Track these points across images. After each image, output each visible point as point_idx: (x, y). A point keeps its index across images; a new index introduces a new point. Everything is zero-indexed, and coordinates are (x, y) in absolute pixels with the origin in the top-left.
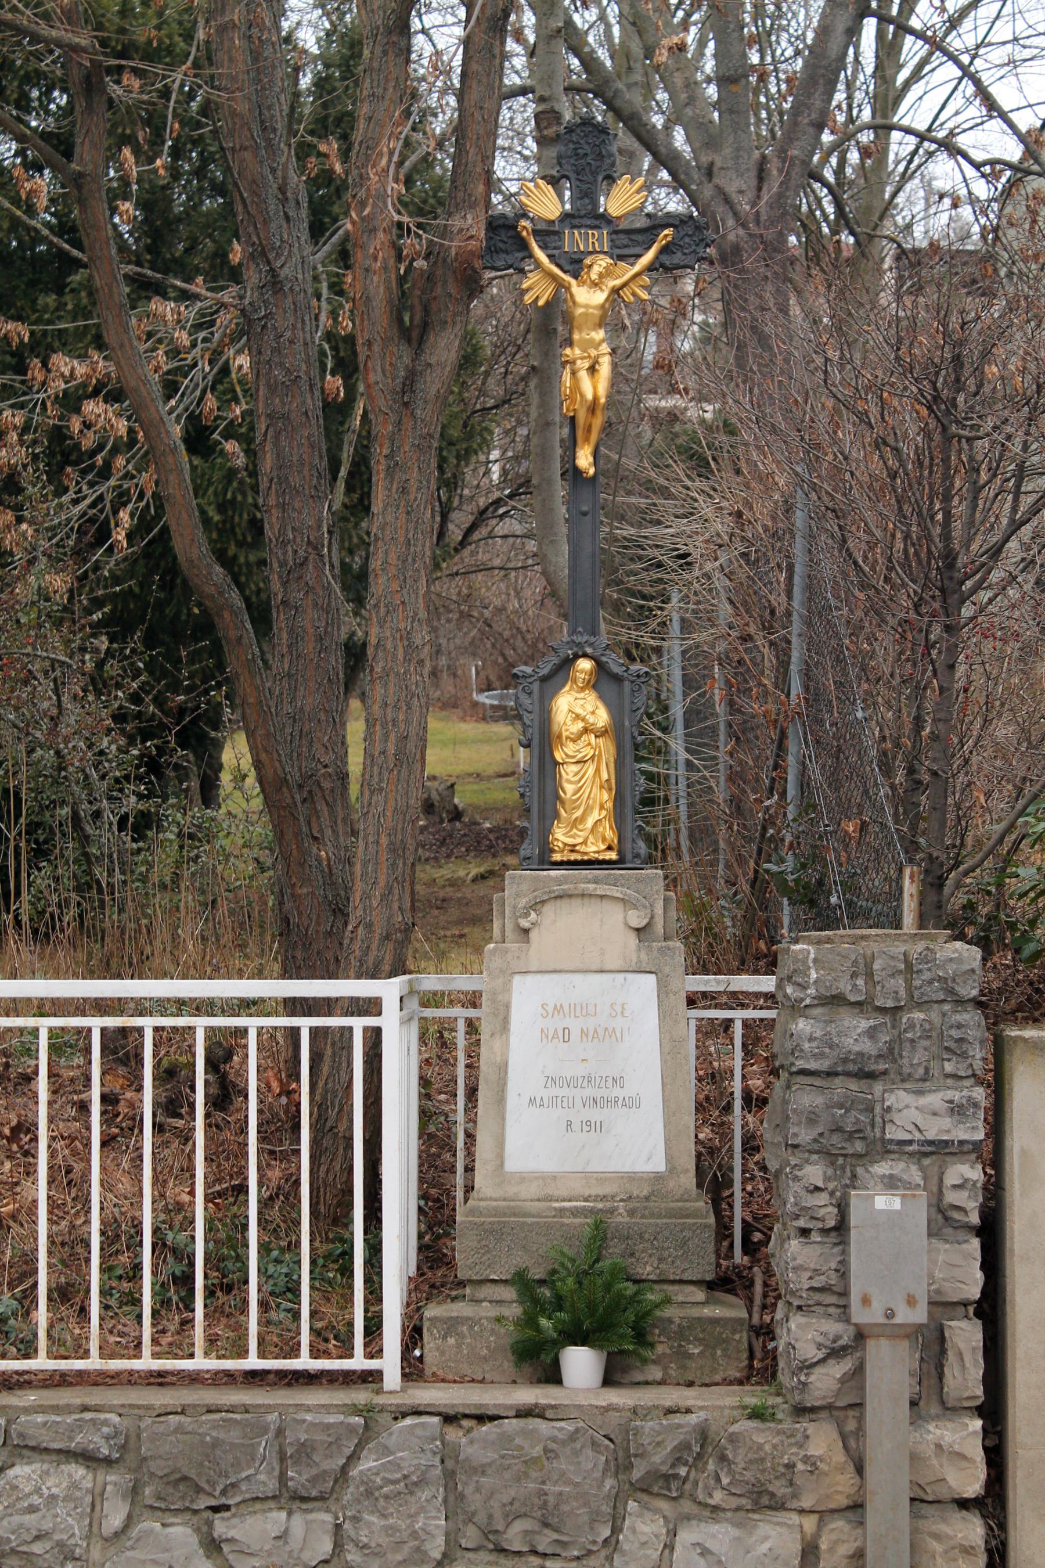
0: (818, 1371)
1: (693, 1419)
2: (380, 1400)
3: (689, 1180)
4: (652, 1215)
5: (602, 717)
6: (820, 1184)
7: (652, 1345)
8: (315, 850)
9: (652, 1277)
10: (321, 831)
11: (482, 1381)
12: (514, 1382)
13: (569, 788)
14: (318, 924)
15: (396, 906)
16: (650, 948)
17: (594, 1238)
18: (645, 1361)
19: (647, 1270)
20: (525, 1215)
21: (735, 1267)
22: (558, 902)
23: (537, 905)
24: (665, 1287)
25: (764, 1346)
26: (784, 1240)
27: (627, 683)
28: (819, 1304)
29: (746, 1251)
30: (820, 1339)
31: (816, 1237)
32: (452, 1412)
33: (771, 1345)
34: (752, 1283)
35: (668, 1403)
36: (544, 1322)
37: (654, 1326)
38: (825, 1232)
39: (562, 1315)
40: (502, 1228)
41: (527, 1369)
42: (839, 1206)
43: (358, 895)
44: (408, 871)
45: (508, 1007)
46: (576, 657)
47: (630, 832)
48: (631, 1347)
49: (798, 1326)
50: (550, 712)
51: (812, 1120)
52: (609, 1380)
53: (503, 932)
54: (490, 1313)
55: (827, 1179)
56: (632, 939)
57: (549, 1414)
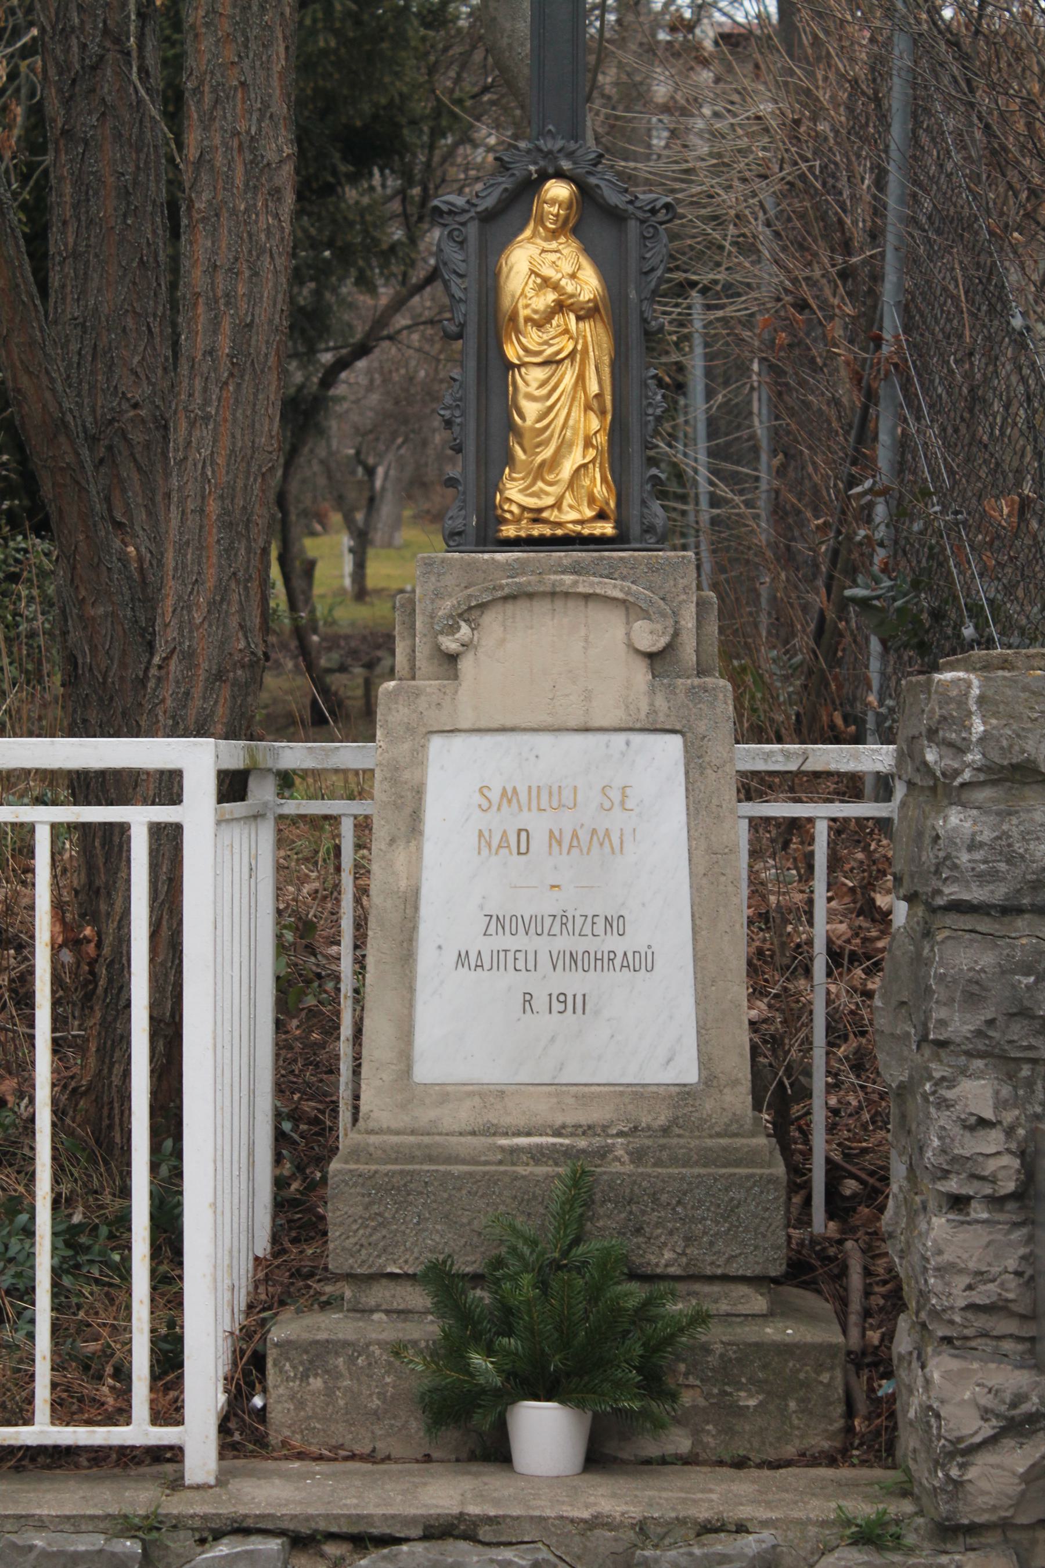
0: (984, 1460)
1: (750, 1544)
2: (175, 1505)
3: (738, 1099)
4: (674, 1161)
5: (588, 284)
6: (988, 1114)
7: (674, 1397)
8: (117, 544)
9: (672, 1270)
10: (128, 512)
11: (370, 1458)
12: (428, 1459)
13: (531, 409)
14: (123, 665)
15: (234, 622)
16: (671, 690)
17: (571, 1202)
18: (659, 1426)
19: (664, 1258)
20: (449, 1160)
21: (813, 1242)
22: (510, 607)
23: (471, 612)
24: (697, 1287)
25: (872, 1390)
26: (915, 1212)
27: (632, 224)
28: (984, 1335)
29: (831, 1213)
30: (987, 1401)
31: (979, 1212)
32: (305, 1530)
33: (886, 1388)
34: (844, 1271)
35: (703, 1514)
36: (477, 1360)
37: (679, 1358)
38: (996, 1202)
39: (510, 1343)
40: (415, 1179)
41: (451, 1435)
42: (1022, 1154)
43: (170, 602)
44: (255, 562)
45: (419, 791)
46: (544, 177)
47: (636, 490)
48: (636, 1406)
49: (946, 1375)
50: (497, 275)
51: (973, 994)
52: (597, 1458)
53: (412, 660)
54: (389, 1329)
55: (1000, 1105)
56: (641, 674)
57: (485, 1533)
